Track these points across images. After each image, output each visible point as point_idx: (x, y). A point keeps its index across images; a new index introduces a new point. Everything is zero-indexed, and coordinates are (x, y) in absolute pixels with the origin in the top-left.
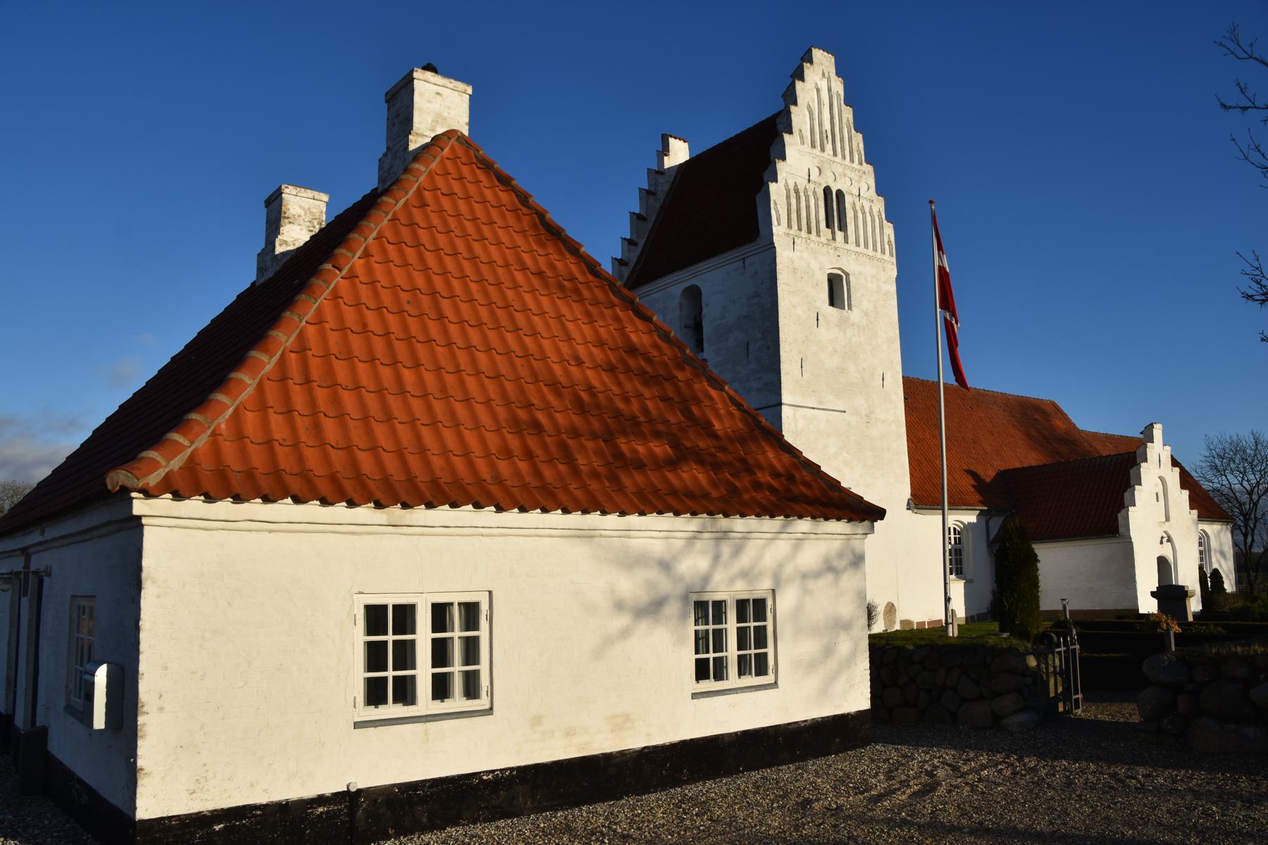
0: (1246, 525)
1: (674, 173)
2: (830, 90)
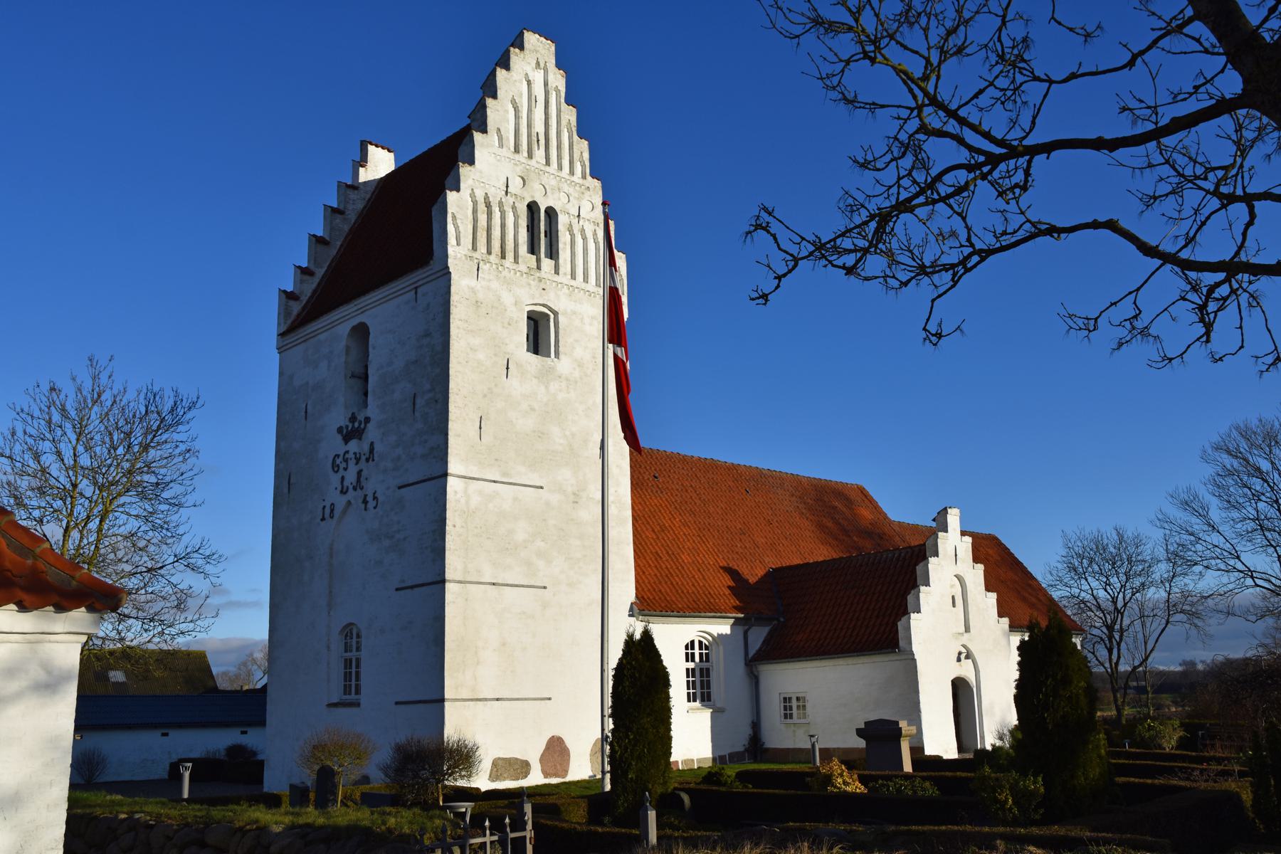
0: (1111, 637)
1: (371, 189)
2: (546, 84)
